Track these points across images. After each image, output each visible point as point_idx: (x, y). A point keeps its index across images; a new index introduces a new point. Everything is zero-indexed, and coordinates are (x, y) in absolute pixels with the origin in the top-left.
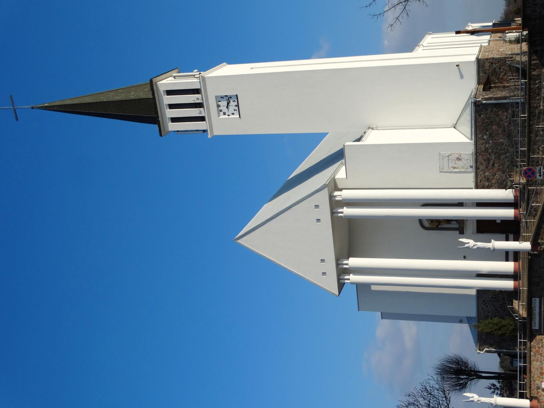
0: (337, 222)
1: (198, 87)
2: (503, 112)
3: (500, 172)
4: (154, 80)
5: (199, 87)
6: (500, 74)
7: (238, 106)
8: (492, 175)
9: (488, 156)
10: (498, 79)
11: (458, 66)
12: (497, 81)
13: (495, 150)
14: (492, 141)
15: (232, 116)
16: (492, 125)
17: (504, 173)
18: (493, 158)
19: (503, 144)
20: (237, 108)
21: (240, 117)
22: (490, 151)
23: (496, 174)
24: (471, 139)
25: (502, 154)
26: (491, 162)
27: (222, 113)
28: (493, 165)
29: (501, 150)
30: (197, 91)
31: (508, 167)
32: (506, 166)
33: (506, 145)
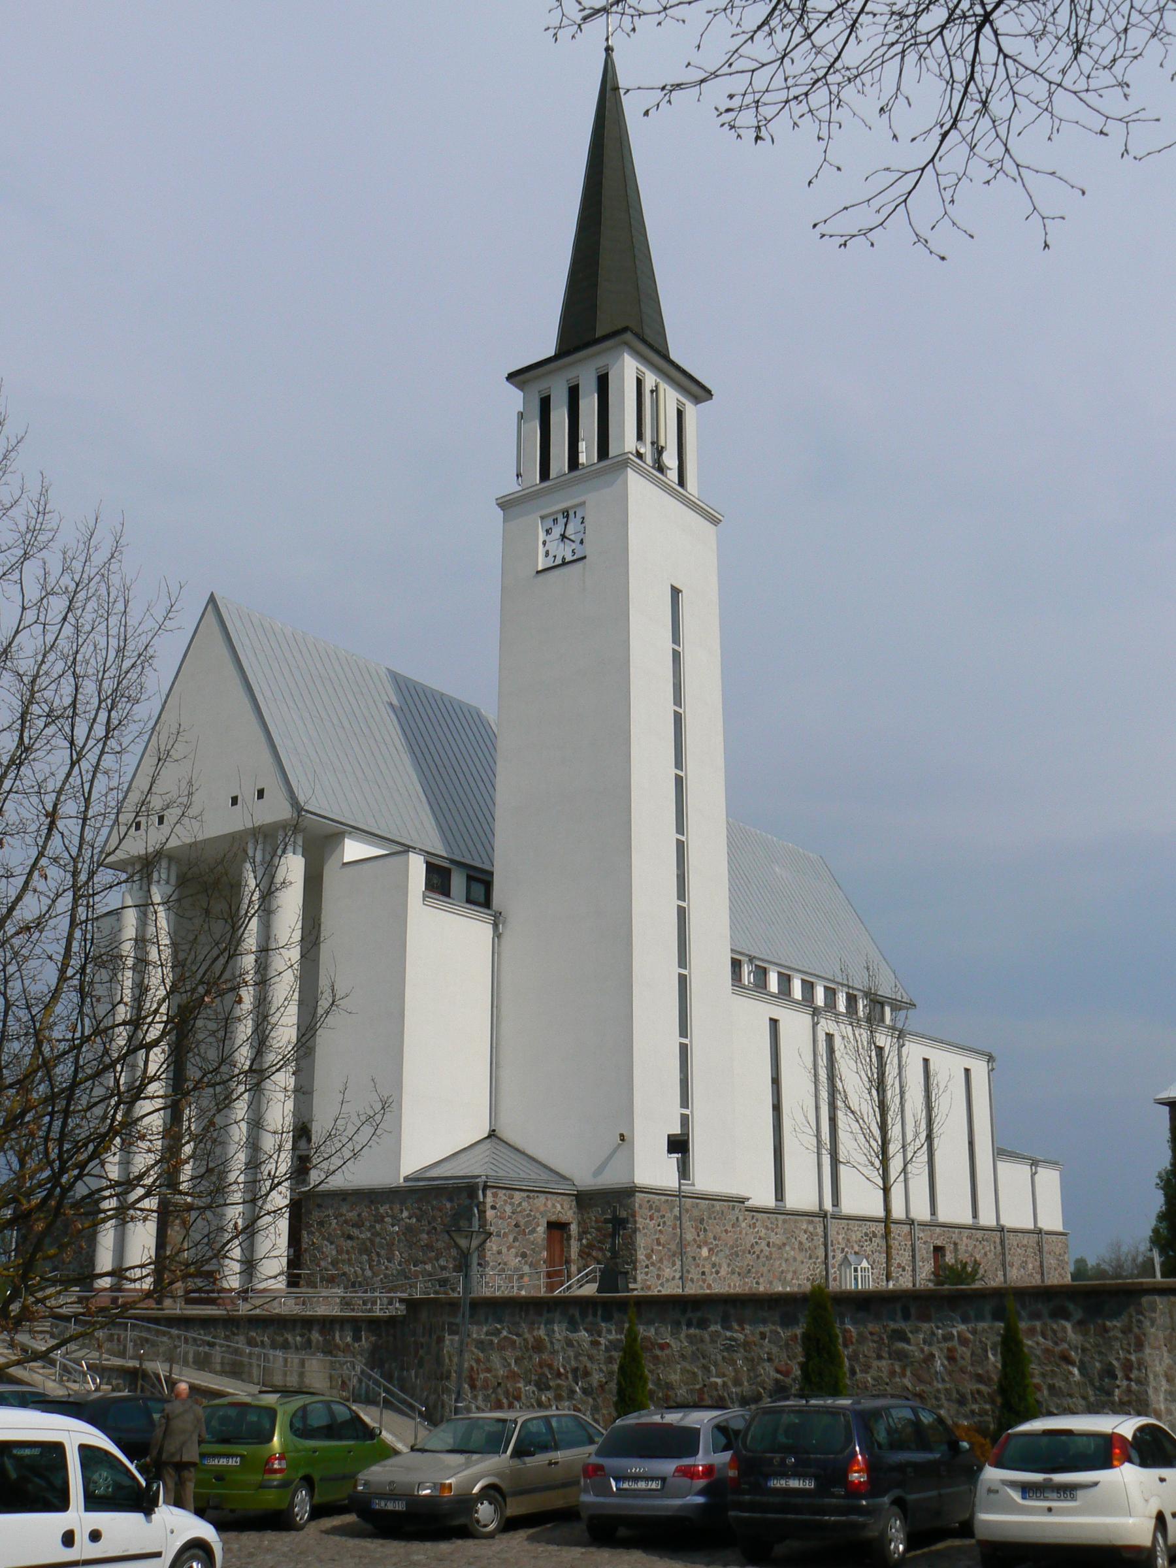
0: (234, 849)
1: (612, 453)
2: (455, 1259)
3: (334, 1253)
4: (628, 336)
5: (611, 455)
6: (601, 1249)
7: (564, 563)
8: (330, 1234)
9: (368, 1224)
10: (590, 1246)
11: (622, 1137)
12: (584, 1241)
13: (378, 1240)
14: (397, 1233)
15: (541, 551)
16: (428, 1233)
17: (332, 1263)
18: (363, 1236)
19: (389, 1261)
20: (559, 561)
21: (538, 572)
22: (378, 1227)
23: (332, 1243)
24: (406, 1179)
25: (370, 1260)
26: (355, 1232)
27: (549, 523)
28: (350, 1237)
29: (378, 1255)
30: (603, 452)
31: (344, 1274)
32: (346, 1269)
33: (387, 1268)
